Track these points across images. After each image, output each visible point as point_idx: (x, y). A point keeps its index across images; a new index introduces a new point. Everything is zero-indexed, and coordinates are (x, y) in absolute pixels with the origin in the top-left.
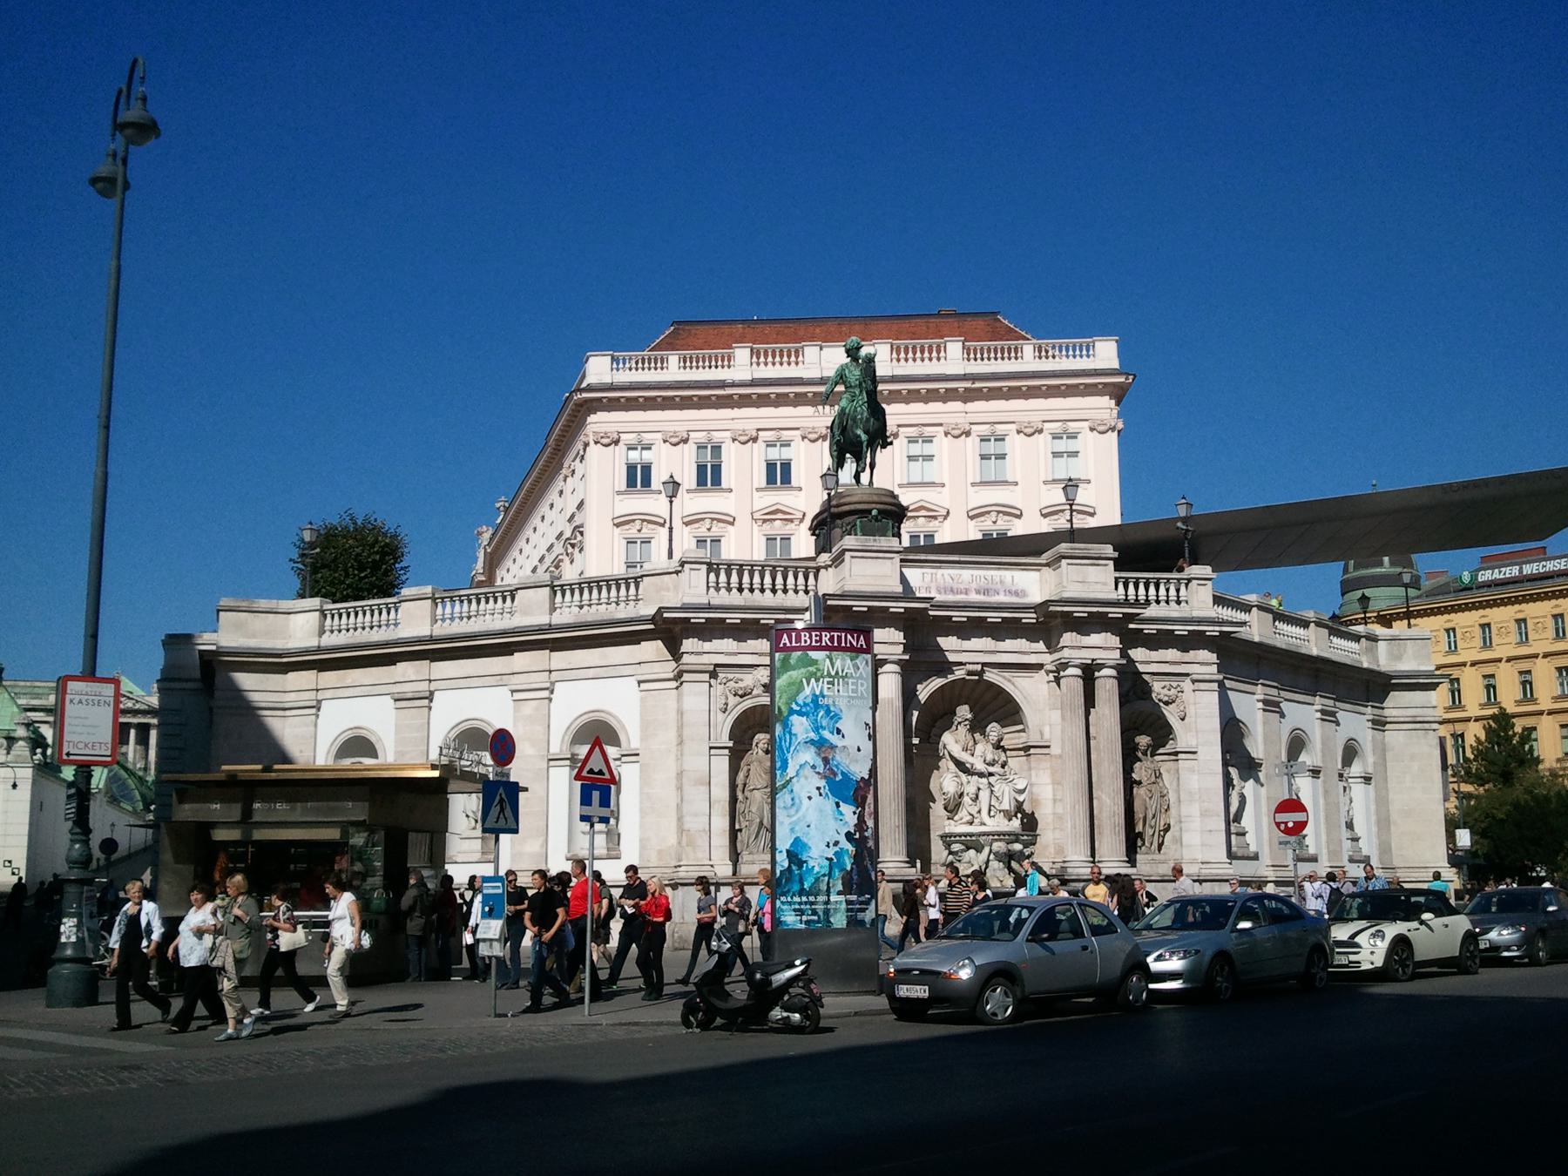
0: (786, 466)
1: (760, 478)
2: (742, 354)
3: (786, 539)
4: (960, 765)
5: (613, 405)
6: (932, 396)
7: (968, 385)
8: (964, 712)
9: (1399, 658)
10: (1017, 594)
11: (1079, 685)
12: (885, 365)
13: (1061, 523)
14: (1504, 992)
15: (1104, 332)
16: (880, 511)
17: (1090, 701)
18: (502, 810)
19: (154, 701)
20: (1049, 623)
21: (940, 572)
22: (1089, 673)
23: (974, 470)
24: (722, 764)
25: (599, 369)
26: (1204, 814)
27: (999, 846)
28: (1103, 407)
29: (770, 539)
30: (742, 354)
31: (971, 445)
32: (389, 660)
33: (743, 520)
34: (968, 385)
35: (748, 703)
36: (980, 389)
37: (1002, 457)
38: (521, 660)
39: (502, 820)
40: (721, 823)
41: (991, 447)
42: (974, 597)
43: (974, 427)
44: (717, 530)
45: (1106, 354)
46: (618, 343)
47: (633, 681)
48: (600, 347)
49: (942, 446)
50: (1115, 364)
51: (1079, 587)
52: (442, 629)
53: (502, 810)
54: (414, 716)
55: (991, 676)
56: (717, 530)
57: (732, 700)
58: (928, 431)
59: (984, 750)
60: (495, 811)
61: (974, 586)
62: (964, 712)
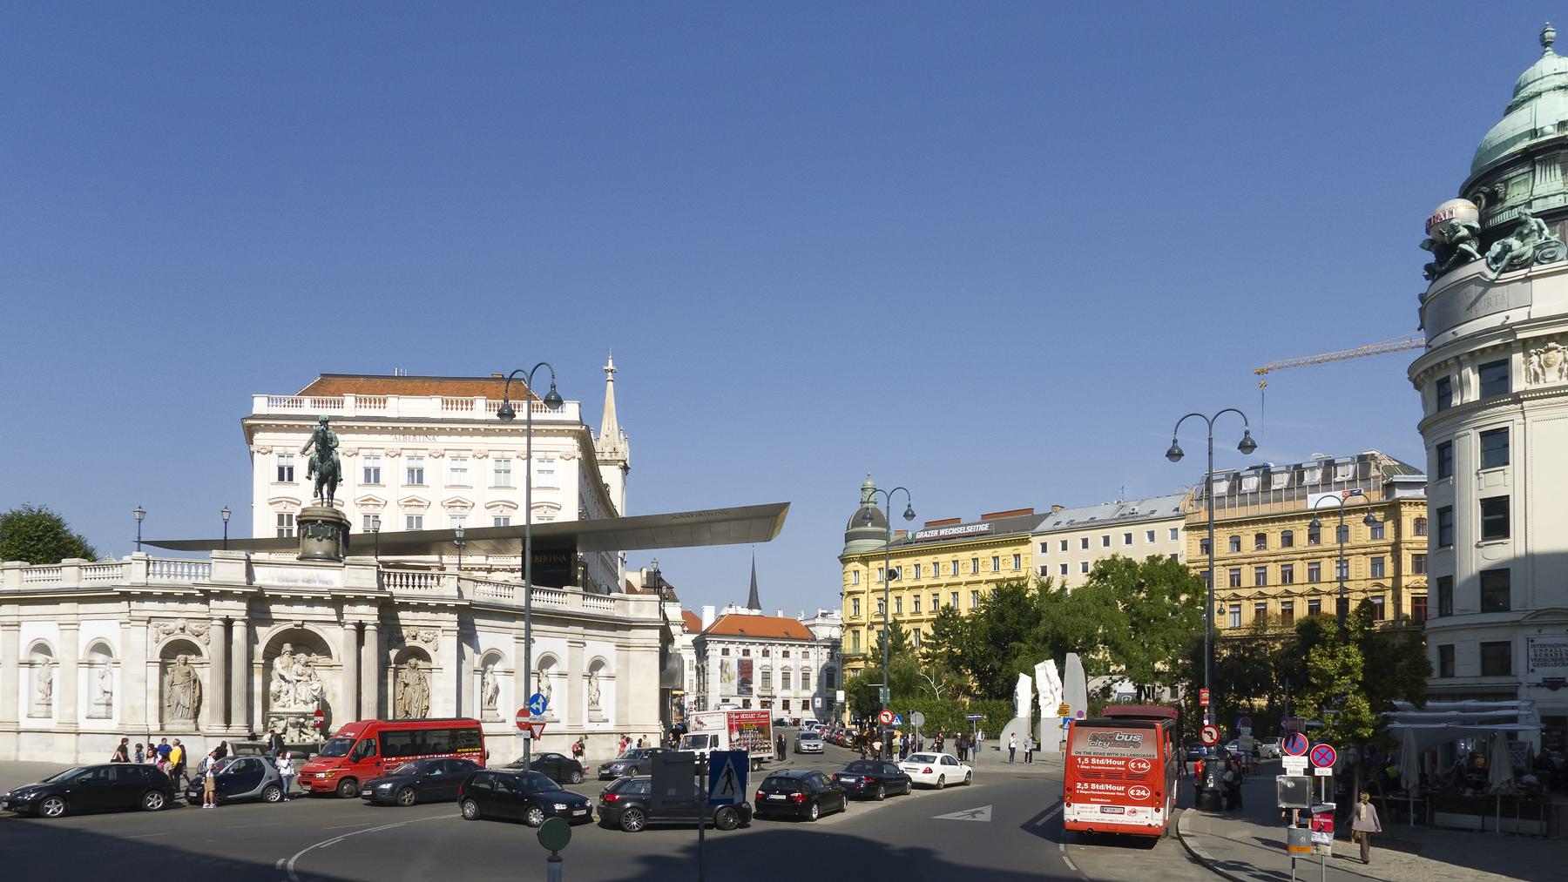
1: (404, 478)
3: (419, 519)
4: (282, 677)
5: (267, 428)
6: (464, 432)
8: (287, 647)
11: (353, 635)
13: (257, 556)
17: (360, 641)
18: (729, 780)
19: (402, 614)
20: (338, 601)
22: (360, 628)
23: (491, 479)
24: (155, 671)
25: (260, 405)
26: (446, 701)
27: (292, 720)
31: (490, 464)
32: (56, 601)
33: (392, 503)
35: (172, 638)
37: (508, 472)
38: (64, 607)
39: (729, 791)
41: (502, 466)
42: (300, 584)
44: (377, 510)
46: (271, 389)
47: (116, 623)
48: (261, 392)
49: (471, 463)
52: (84, 584)
53: (729, 780)
55: (307, 626)
56: (377, 510)
57: (162, 636)
58: (464, 454)
59: (298, 668)
60: (722, 782)
62: (287, 647)
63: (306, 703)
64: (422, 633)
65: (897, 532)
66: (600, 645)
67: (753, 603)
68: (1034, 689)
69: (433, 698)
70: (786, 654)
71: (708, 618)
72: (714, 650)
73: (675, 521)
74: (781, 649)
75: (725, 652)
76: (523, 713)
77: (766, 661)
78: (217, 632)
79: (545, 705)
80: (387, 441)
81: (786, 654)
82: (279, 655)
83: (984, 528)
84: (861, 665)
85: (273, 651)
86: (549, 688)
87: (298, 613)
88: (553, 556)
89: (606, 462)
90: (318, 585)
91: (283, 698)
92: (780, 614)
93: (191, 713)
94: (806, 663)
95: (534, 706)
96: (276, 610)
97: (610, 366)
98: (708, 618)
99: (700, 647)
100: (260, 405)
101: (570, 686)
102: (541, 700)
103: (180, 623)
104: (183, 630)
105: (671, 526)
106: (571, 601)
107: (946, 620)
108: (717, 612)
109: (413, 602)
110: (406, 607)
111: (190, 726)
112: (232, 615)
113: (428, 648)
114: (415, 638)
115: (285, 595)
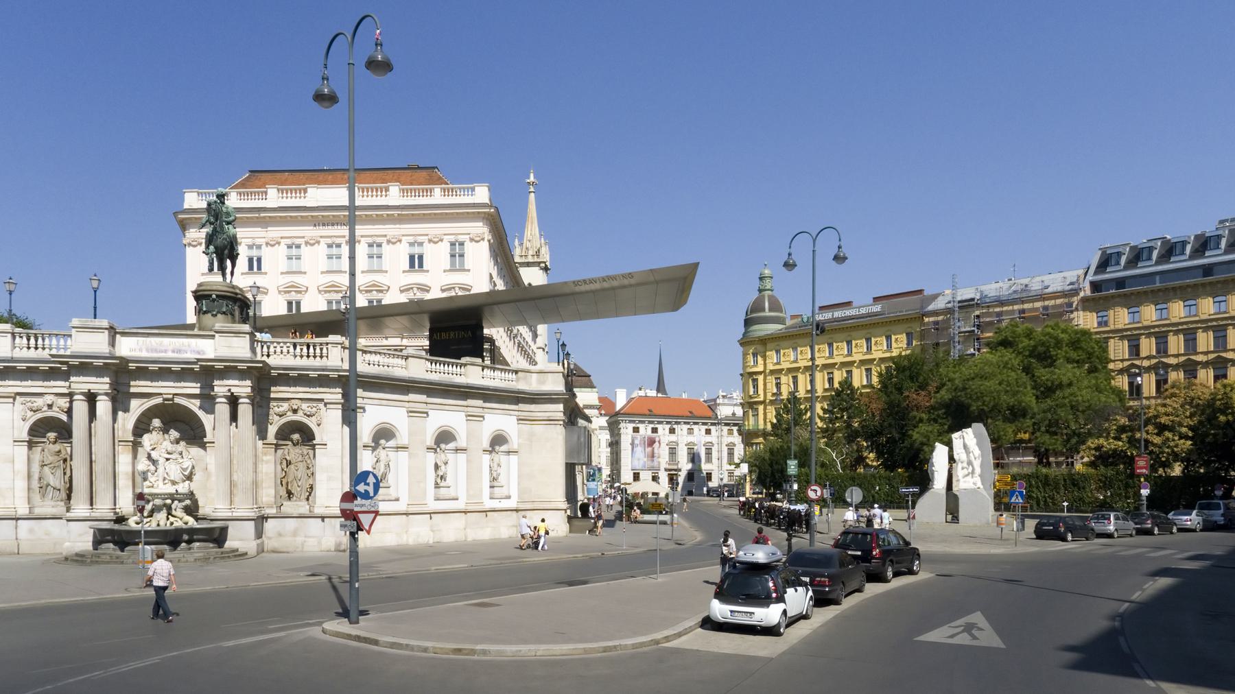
0: (421, 257)
2: (272, 192)
4: (149, 457)
9: (543, 383)
10: (199, 353)
12: (234, 201)
22: (233, 401)
26: (330, 479)
29: (290, 303)
30: (272, 192)
33: (273, 291)
35: (39, 416)
43: (404, 238)
45: (481, 194)
50: (487, 201)
55: (177, 400)
56: (298, 297)
57: (30, 413)
61: (171, 348)
62: (156, 423)
63: (174, 483)
64: (304, 406)
65: (793, 317)
66: (500, 419)
67: (660, 387)
68: (952, 459)
69: (318, 476)
71: (621, 400)
72: (626, 430)
73: (578, 289)
74: (685, 427)
75: (636, 430)
76: (349, 497)
77: (673, 438)
78: (80, 408)
79: (377, 487)
80: (309, 232)
82: (148, 431)
83: (877, 308)
84: (761, 440)
85: (141, 428)
86: (499, 465)
87: (166, 388)
88: (456, 330)
89: (528, 264)
90: (170, 355)
91: (152, 478)
92: (684, 396)
93: (64, 495)
94: (708, 438)
95: (361, 488)
96: (138, 386)
97: (532, 178)
98: (621, 400)
99: (613, 427)
101: (468, 461)
102: (371, 480)
103: (49, 399)
104: (50, 406)
105: (573, 294)
106: (472, 373)
107: (843, 397)
108: (628, 395)
111: (60, 509)
112: (94, 388)
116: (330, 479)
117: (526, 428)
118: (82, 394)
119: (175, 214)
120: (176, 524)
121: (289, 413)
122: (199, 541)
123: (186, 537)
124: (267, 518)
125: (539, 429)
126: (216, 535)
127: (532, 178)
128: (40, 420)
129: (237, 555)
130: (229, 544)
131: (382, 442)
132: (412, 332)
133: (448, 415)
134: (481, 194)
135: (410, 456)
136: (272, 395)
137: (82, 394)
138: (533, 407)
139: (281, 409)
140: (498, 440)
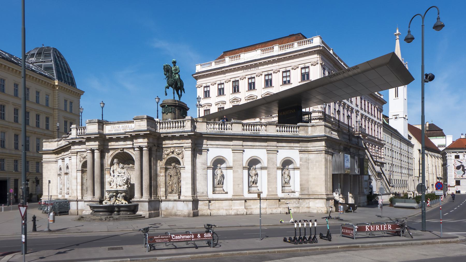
0: (271, 81)
7: (278, 58)
14: (96, 235)
15: (315, 35)
16: (168, 105)
21: (116, 126)
24: (79, 174)
26: (187, 183)
28: (316, 58)
34: (278, 58)
36: (281, 58)
40: (79, 187)
43: (281, 70)
51: (138, 127)
54: (238, 155)
55: (125, 151)
57: (82, 159)
63: (120, 186)
64: (176, 150)
70: (457, 157)
81: (457, 157)
87: (121, 144)
96: (112, 145)
97: (398, 32)
100: (199, 68)
104: (173, 152)
109: (170, 135)
110: (167, 138)
113: (179, 158)
114: (173, 152)
115: (114, 137)
116: (187, 183)
117: (305, 156)
118: (137, 148)
119: (192, 75)
120: (118, 203)
121: (170, 154)
122: (124, 211)
123: (116, 209)
124: (161, 201)
125: (312, 156)
126: (132, 208)
127: (398, 32)
128: (169, 158)
129: (140, 217)
130: (138, 213)
131: (219, 165)
132: (269, 114)
133: (286, 152)
134: (317, 41)
135: (301, 172)
136: (110, 147)
137: (137, 148)
138: (309, 144)
139: (167, 152)
140: (287, 163)
